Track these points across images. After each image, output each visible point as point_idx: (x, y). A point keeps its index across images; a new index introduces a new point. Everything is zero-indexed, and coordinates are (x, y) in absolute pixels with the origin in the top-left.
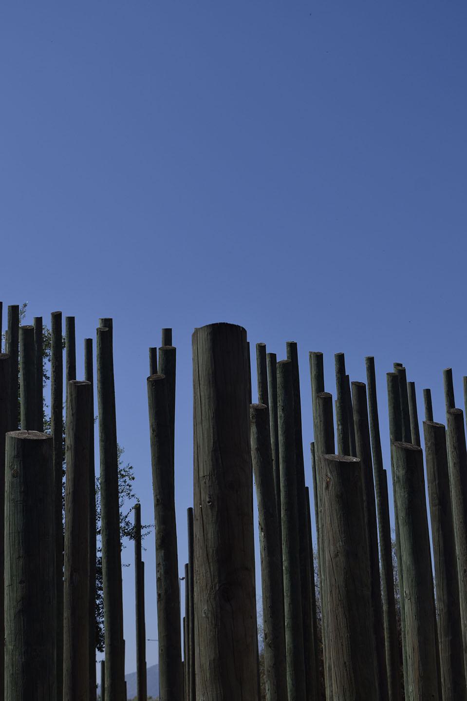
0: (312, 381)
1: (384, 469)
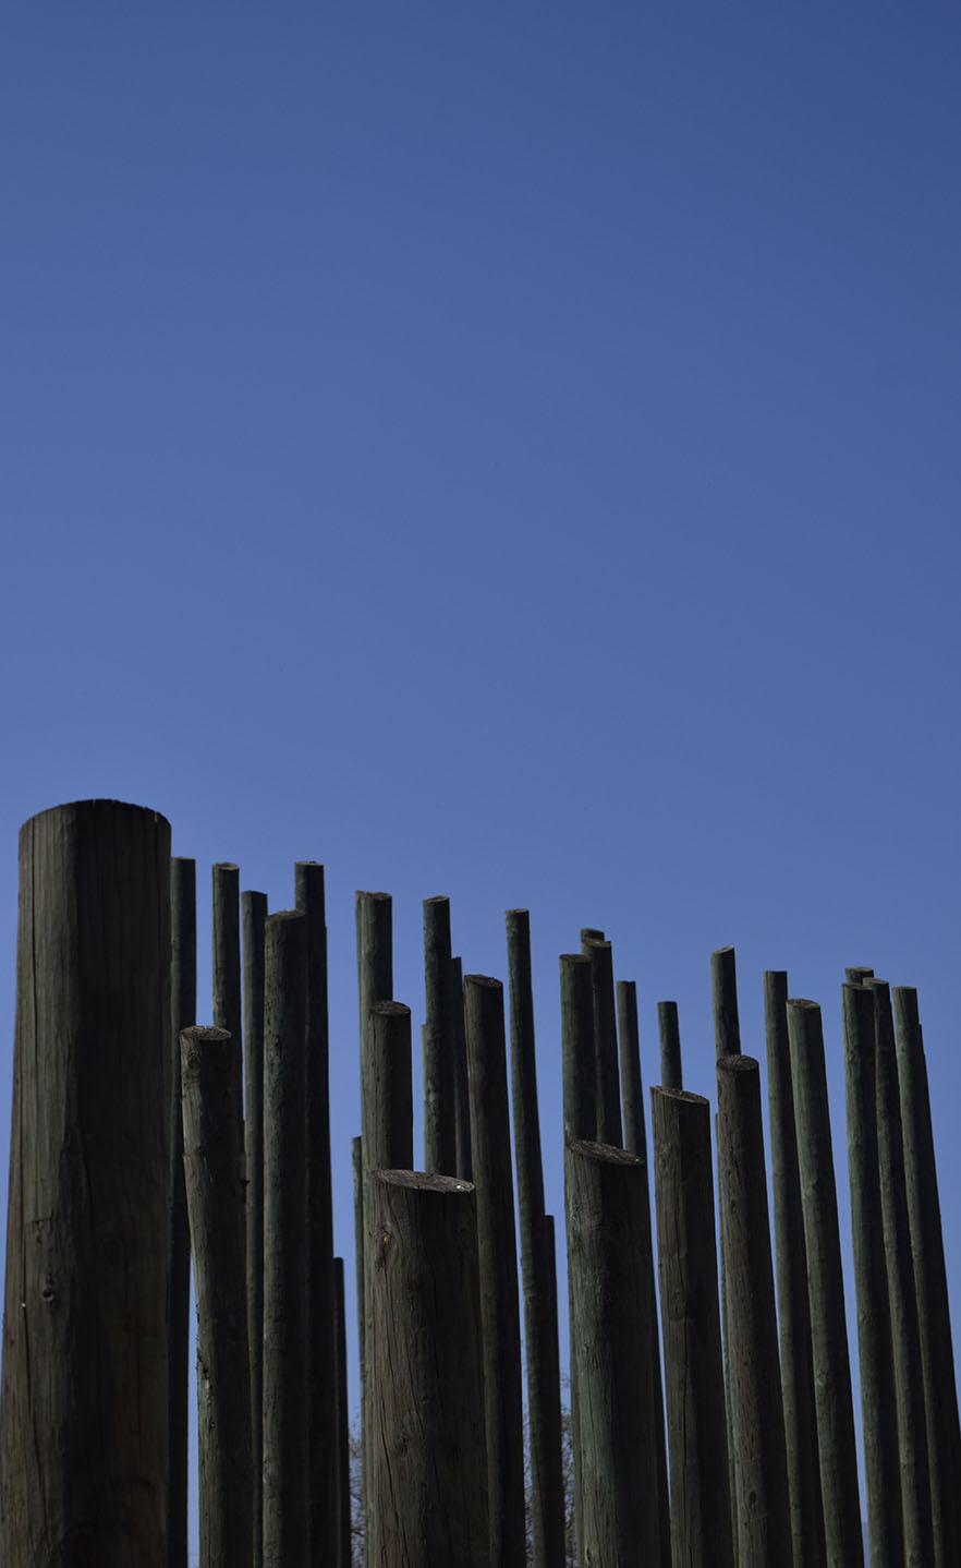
0: (360, 968)
1: (547, 1213)
